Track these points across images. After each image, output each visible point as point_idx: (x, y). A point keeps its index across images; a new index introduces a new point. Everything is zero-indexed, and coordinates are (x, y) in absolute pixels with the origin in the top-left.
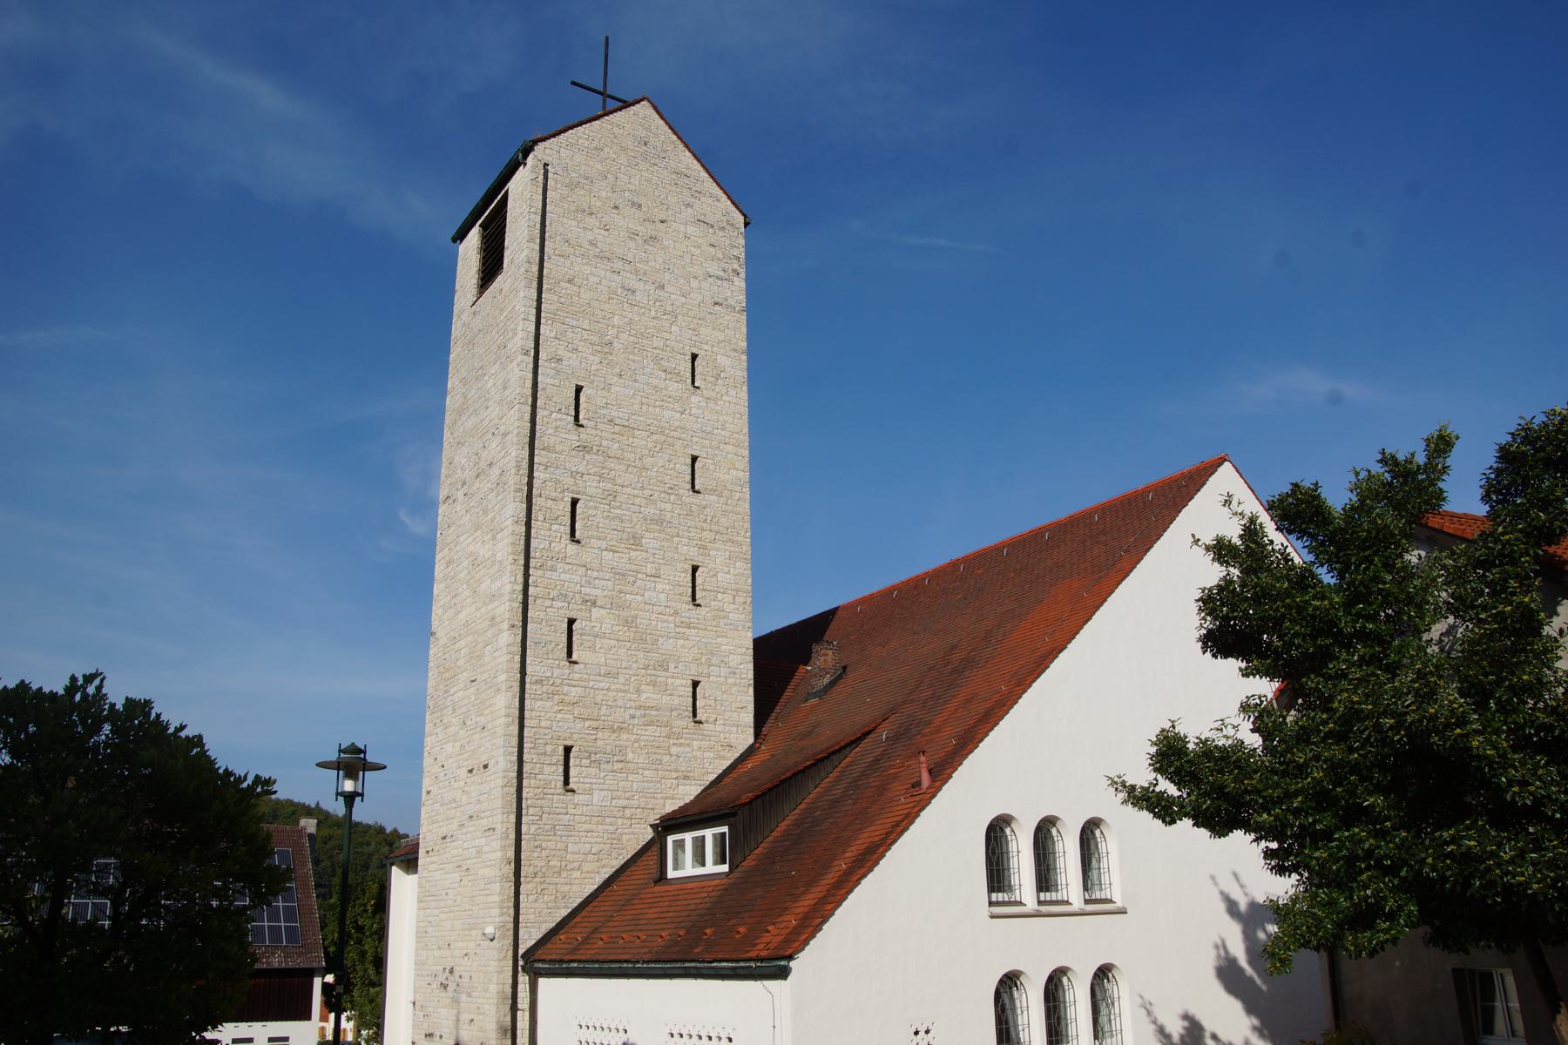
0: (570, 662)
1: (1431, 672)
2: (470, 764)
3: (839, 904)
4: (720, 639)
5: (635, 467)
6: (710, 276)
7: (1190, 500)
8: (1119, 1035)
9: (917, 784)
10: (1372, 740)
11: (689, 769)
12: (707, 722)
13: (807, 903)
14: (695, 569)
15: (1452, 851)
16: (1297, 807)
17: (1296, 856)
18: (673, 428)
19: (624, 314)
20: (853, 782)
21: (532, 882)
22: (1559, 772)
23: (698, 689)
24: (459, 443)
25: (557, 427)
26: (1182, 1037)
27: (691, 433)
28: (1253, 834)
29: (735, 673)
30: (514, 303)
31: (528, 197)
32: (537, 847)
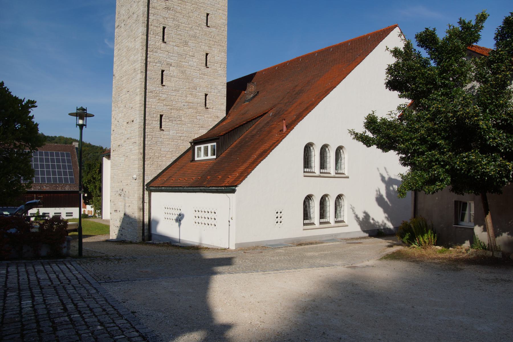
0: (162, 85)
1: (468, 98)
2: (127, 121)
3: (253, 169)
4: (215, 80)
5: (186, 16)
7: (383, 39)
9: (282, 130)
10: (443, 121)
12: (210, 108)
13: (242, 168)
14: (207, 54)
15: (466, 160)
16: (414, 143)
17: (411, 160)
21: (149, 160)
22: (506, 136)
24: (122, 6)
26: (363, 219)
27: (207, 5)
28: (397, 152)
29: (220, 92)
32: (150, 149)
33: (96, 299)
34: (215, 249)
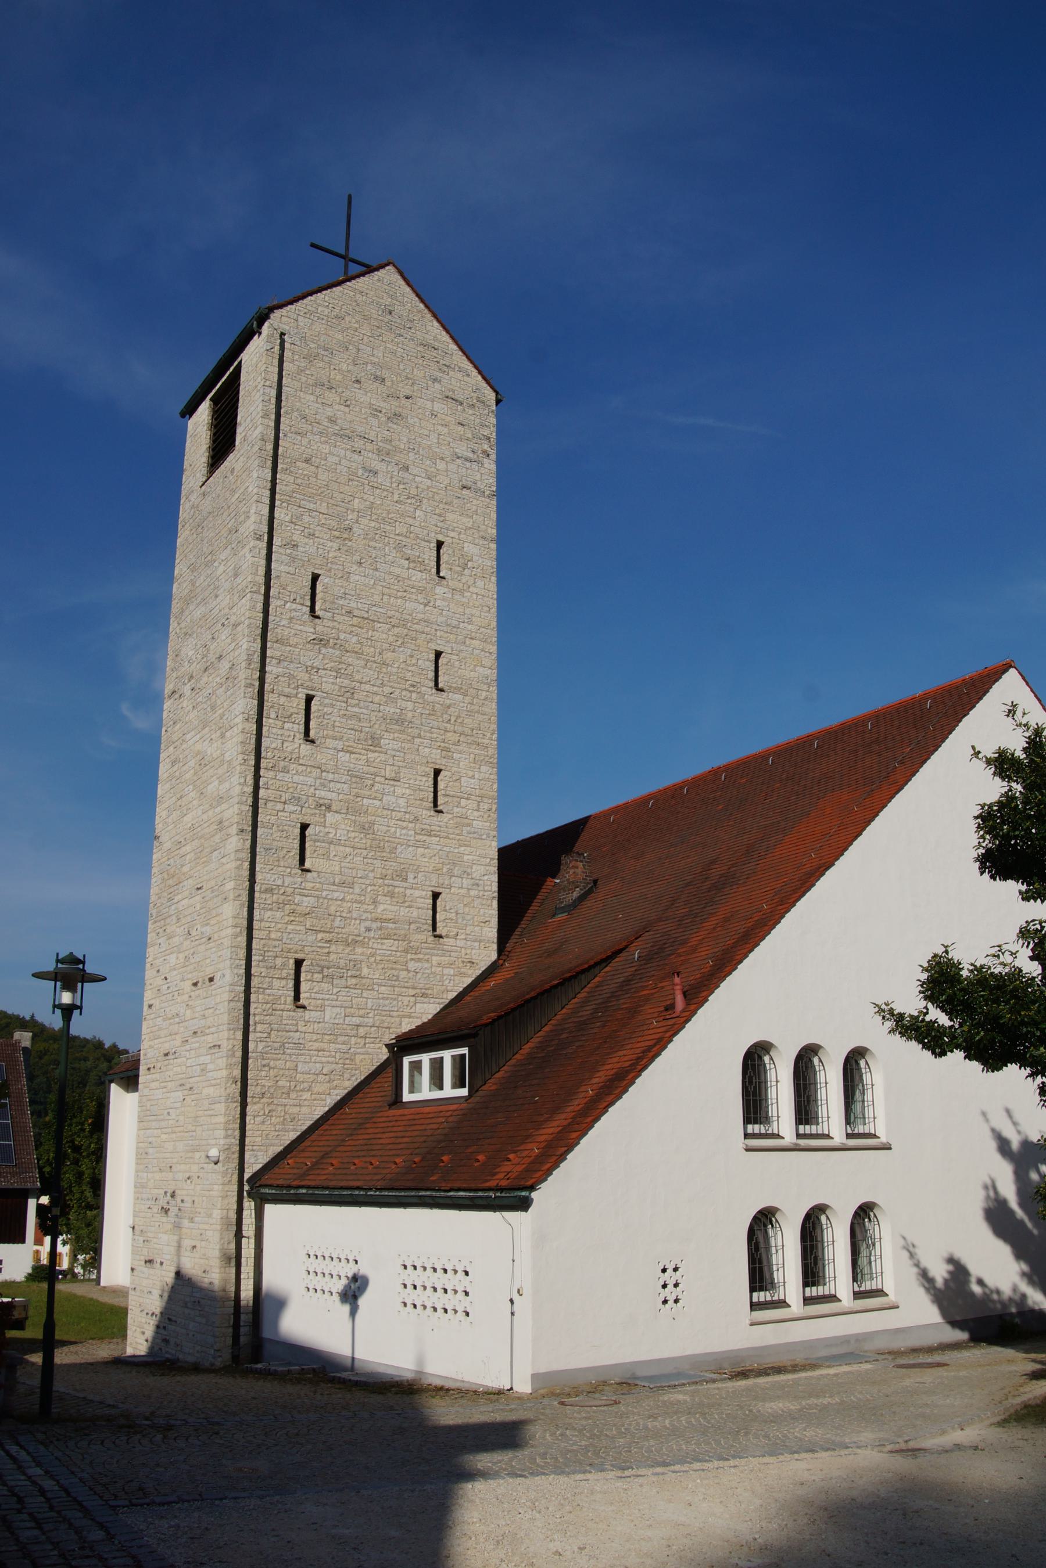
0: (303, 870)
2: (195, 977)
3: (584, 1133)
4: (462, 849)
5: (375, 662)
7: (971, 709)
9: (671, 1007)
11: (427, 986)
12: (447, 936)
13: (552, 1130)
14: (437, 772)
18: (415, 621)
24: (186, 634)
25: (291, 618)
26: (946, 1281)
28: (1028, 1069)
29: (478, 885)
30: (247, 484)
31: (263, 368)
32: (264, 1066)
33: (106, 1559)
34: (467, 1391)
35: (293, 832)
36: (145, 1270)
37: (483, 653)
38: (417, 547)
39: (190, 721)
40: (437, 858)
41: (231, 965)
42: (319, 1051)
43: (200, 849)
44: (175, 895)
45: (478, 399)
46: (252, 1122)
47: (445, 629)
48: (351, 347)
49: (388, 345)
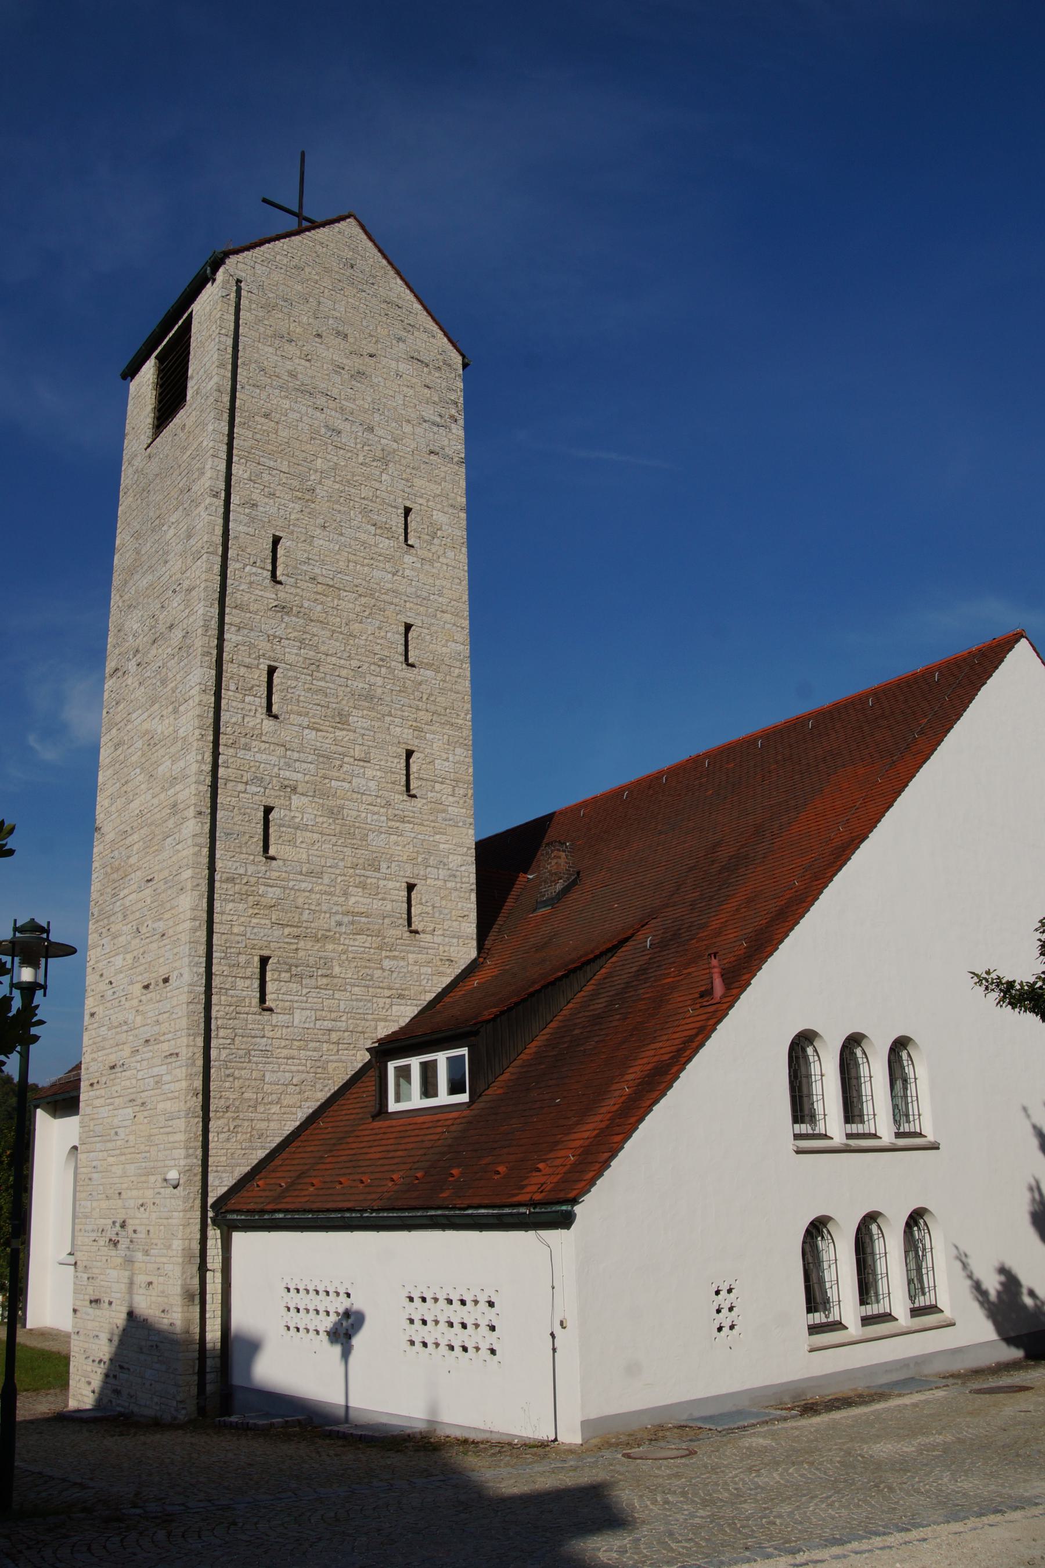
0: (267, 858)
4: (438, 837)
5: (341, 633)
6: (425, 421)
7: (988, 678)
8: (932, 1292)
9: (708, 992)
11: (404, 986)
12: (424, 932)
13: (586, 1135)
14: (409, 754)
18: (383, 591)
19: (329, 457)
20: (617, 994)
23: (413, 895)
24: (130, 607)
25: (251, 583)
26: (999, 1293)
29: (455, 876)
30: (201, 439)
31: (219, 315)
32: (228, 1076)
35: (255, 816)
36: (90, 1311)
37: (454, 627)
38: (384, 513)
39: (137, 699)
40: (411, 846)
41: (190, 962)
42: (288, 1059)
43: (150, 837)
44: (120, 890)
45: (445, 362)
46: (216, 1139)
47: (415, 601)
48: (311, 300)
49: (350, 300)
